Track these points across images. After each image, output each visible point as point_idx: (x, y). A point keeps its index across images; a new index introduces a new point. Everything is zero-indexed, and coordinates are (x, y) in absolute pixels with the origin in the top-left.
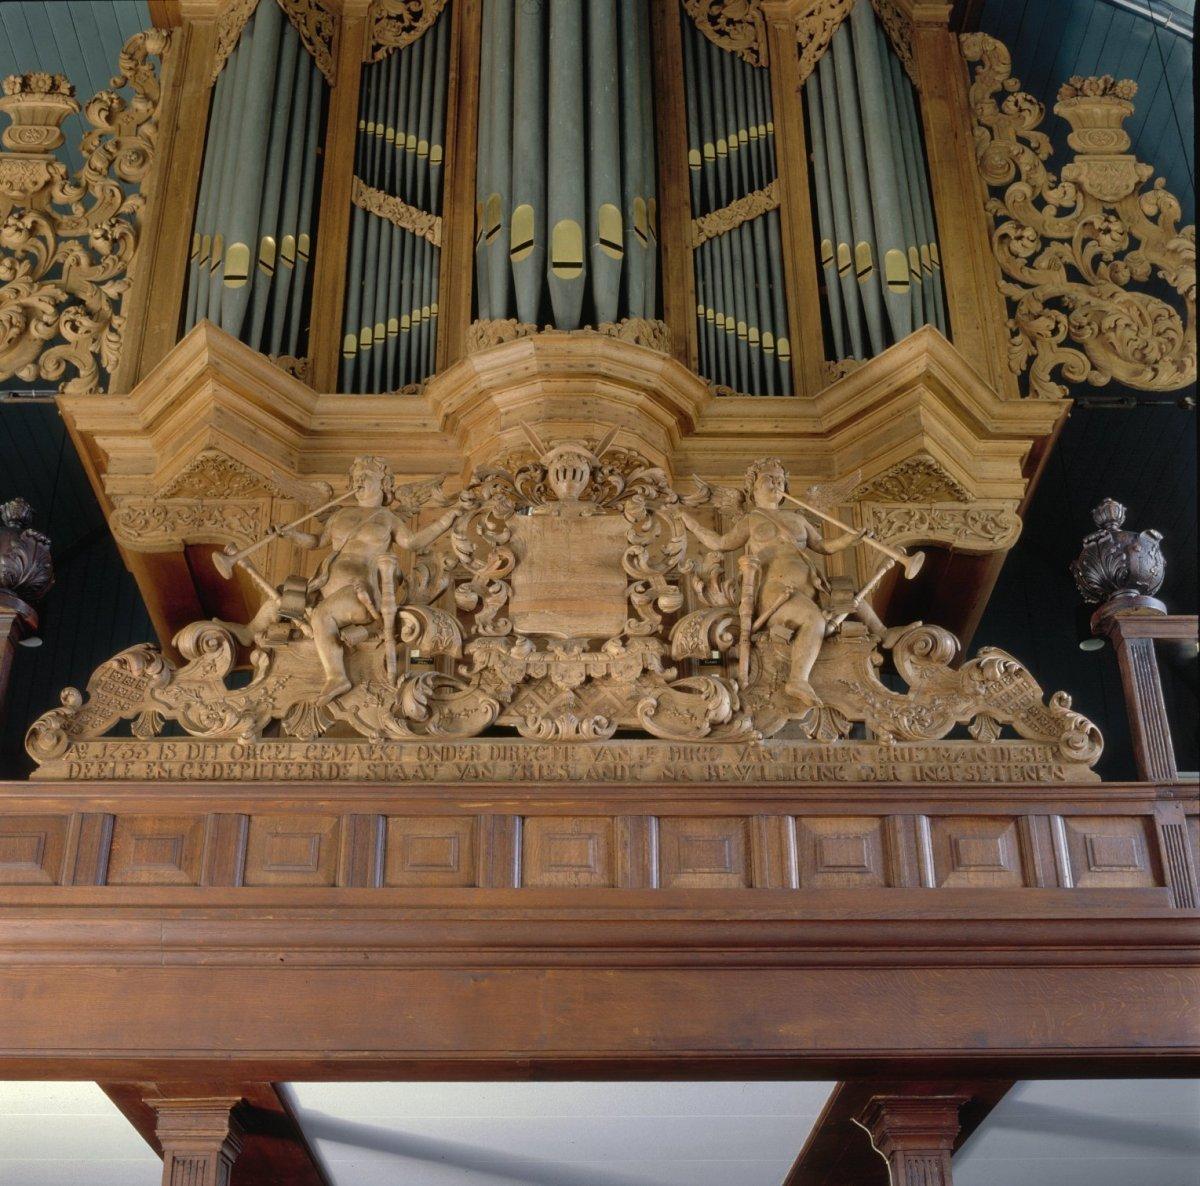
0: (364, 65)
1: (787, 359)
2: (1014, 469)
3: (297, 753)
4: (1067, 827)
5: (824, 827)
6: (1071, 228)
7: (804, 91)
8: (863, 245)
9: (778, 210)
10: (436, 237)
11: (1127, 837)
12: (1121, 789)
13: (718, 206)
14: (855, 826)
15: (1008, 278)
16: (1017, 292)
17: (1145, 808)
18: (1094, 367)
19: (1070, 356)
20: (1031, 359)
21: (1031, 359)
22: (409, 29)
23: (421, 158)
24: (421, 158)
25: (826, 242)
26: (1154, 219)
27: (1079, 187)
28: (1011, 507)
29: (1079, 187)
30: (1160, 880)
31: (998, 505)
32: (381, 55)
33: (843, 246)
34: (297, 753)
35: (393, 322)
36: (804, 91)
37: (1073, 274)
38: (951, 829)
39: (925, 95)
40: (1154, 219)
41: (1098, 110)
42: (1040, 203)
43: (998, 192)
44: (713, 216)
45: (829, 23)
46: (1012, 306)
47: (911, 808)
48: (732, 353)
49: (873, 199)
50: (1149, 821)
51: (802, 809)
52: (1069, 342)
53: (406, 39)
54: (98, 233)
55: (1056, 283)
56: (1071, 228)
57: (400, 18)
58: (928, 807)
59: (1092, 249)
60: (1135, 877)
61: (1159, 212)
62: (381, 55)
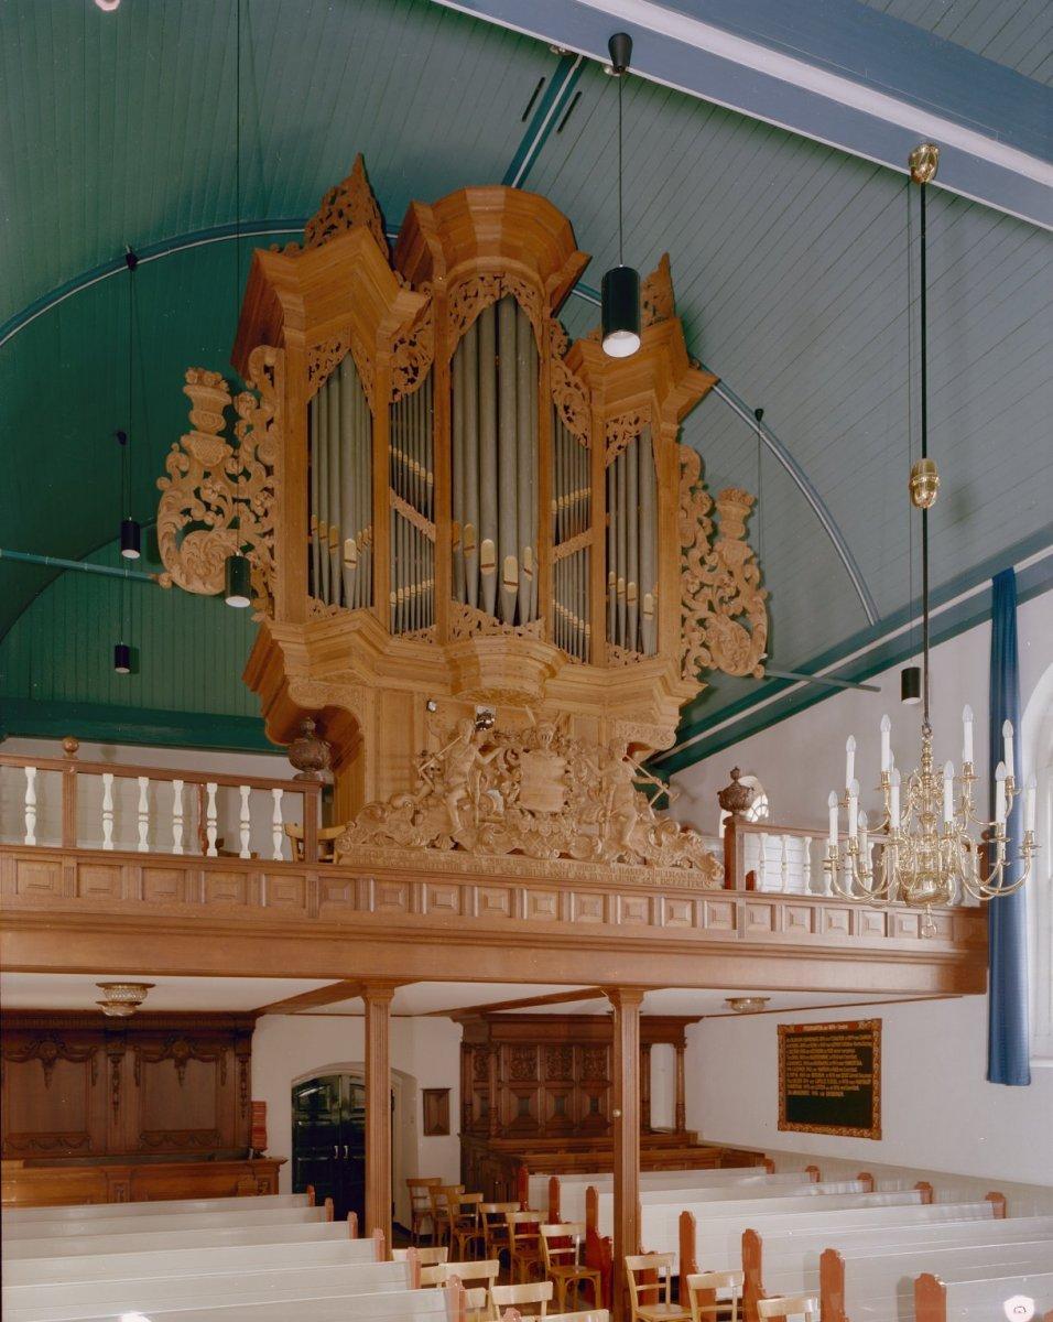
0: (391, 405)
1: (513, 589)
2: (677, 711)
3: (442, 857)
4: (375, 885)
5: (630, 900)
6: (713, 580)
7: (607, 471)
8: (633, 584)
9: (590, 546)
10: (433, 537)
11: (725, 909)
12: (727, 892)
13: (564, 541)
14: (497, 893)
15: (684, 604)
16: (686, 612)
17: (734, 900)
18: (712, 660)
19: (703, 652)
20: (688, 651)
21: (688, 651)
22: (412, 381)
23: (423, 480)
24: (423, 480)
25: (612, 573)
26: (747, 580)
27: (721, 556)
28: (673, 728)
29: (721, 556)
30: (734, 927)
31: (667, 727)
32: (397, 398)
33: (621, 580)
34: (442, 857)
35: (413, 587)
36: (607, 471)
37: (711, 608)
38: (672, 903)
39: (661, 483)
40: (747, 580)
41: (734, 510)
42: (702, 561)
43: (685, 552)
44: (561, 546)
45: (627, 435)
46: (684, 620)
47: (658, 895)
48: (581, 642)
49: (501, 431)
50: (734, 905)
51: (626, 893)
52: (704, 645)
53: (412, 388)
54: (259, 503)
55: (702, 612)
56: (713, 580)
57: (406, 370)
58: (663, 895)
59: (720, 592)
60: (726, 926)
61: (751, 577)
62: (397, 398)
